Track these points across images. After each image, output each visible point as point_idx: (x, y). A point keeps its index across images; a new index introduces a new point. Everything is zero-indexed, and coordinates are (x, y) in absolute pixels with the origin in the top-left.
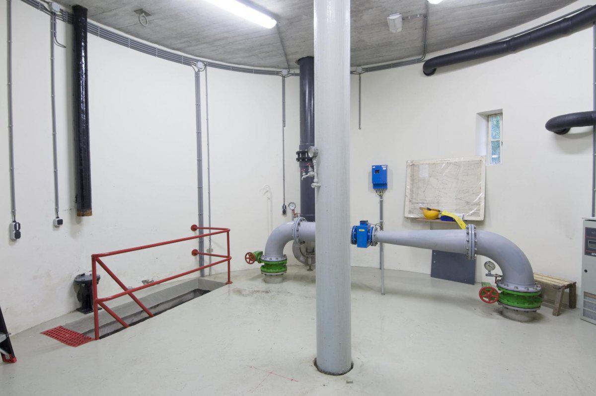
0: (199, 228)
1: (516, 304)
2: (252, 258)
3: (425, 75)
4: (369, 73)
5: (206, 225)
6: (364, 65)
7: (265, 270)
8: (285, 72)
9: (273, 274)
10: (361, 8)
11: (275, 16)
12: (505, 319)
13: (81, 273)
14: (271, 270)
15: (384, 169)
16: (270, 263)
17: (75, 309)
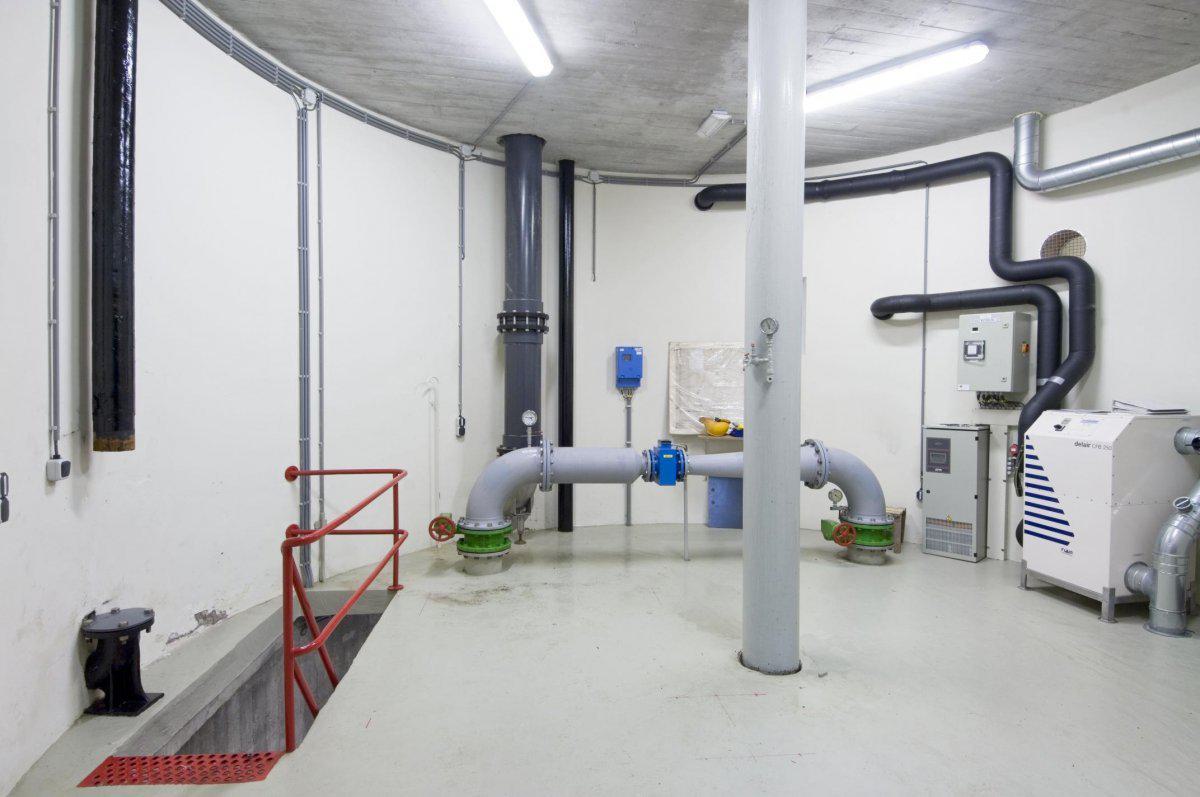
0: (301, 474)
1: (873, 542)
2: (442, 527)
3: (694, 205)
4: (609, 185)
5: (314, 466)
6: (603, 169)
7: (465, 547)
8: (466, 150)
9: (490, 555)
10: (689, 90)
11: (556, 57)
12: (856, 565)
13: (88, 611)
14: (491, 548)
15: (638, 353)
16: (474, 533)
17: (82, 712)
